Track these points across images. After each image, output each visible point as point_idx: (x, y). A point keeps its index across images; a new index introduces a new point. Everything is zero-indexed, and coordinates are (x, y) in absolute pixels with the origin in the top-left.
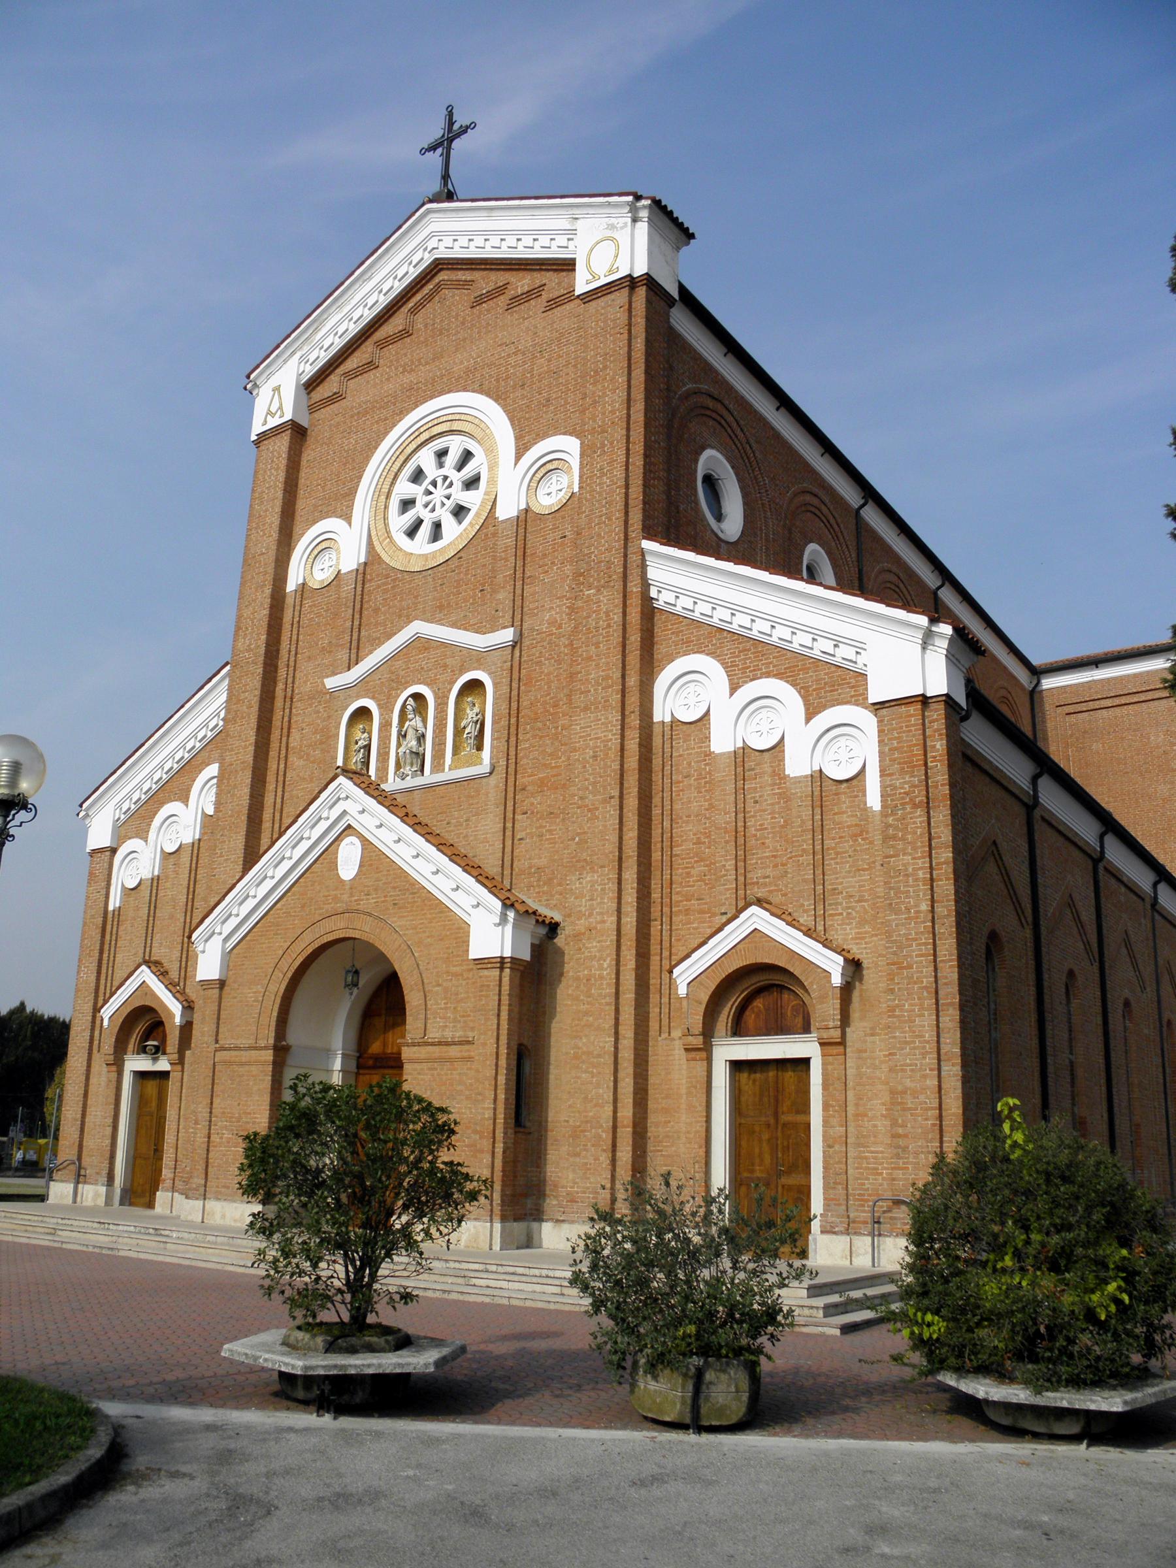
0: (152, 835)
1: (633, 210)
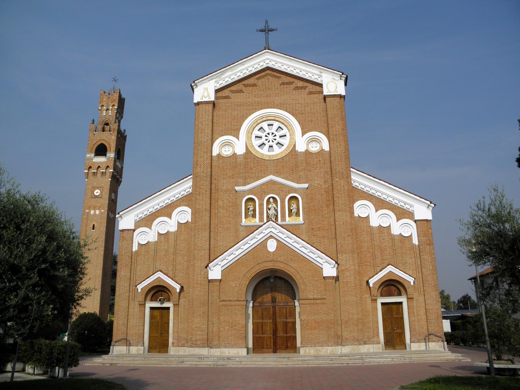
0: (153, 227)
1: (341, 76)
